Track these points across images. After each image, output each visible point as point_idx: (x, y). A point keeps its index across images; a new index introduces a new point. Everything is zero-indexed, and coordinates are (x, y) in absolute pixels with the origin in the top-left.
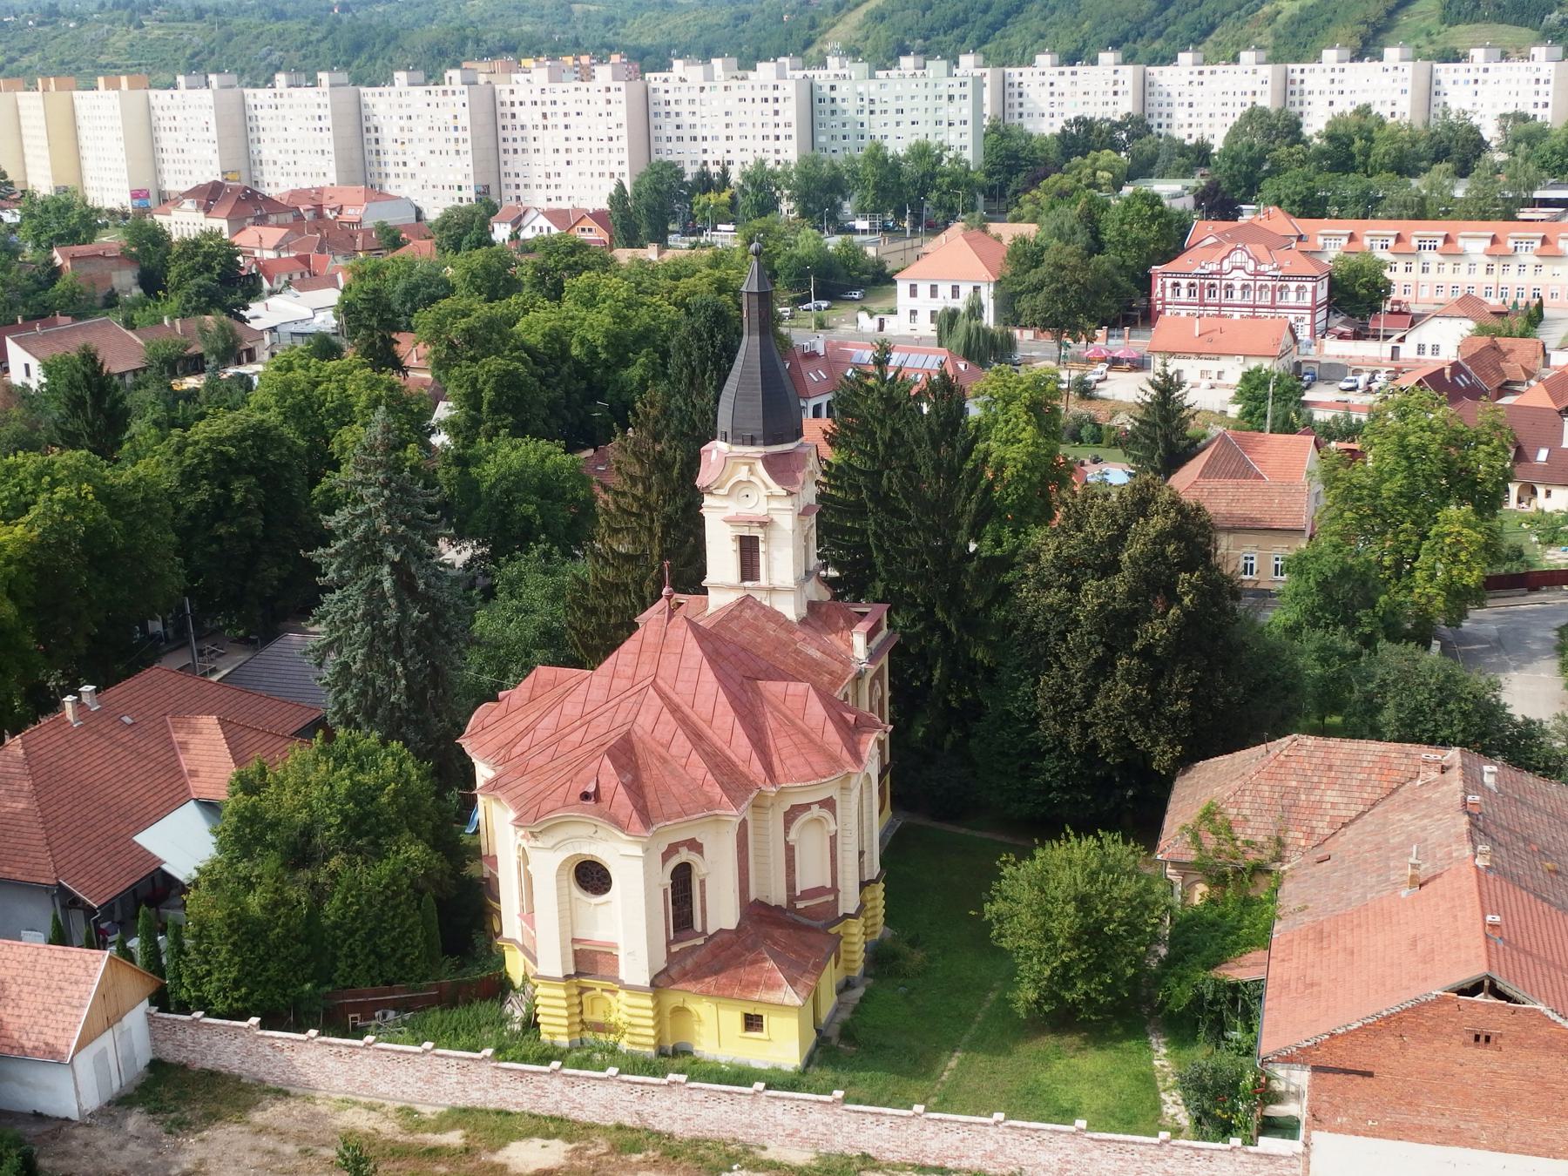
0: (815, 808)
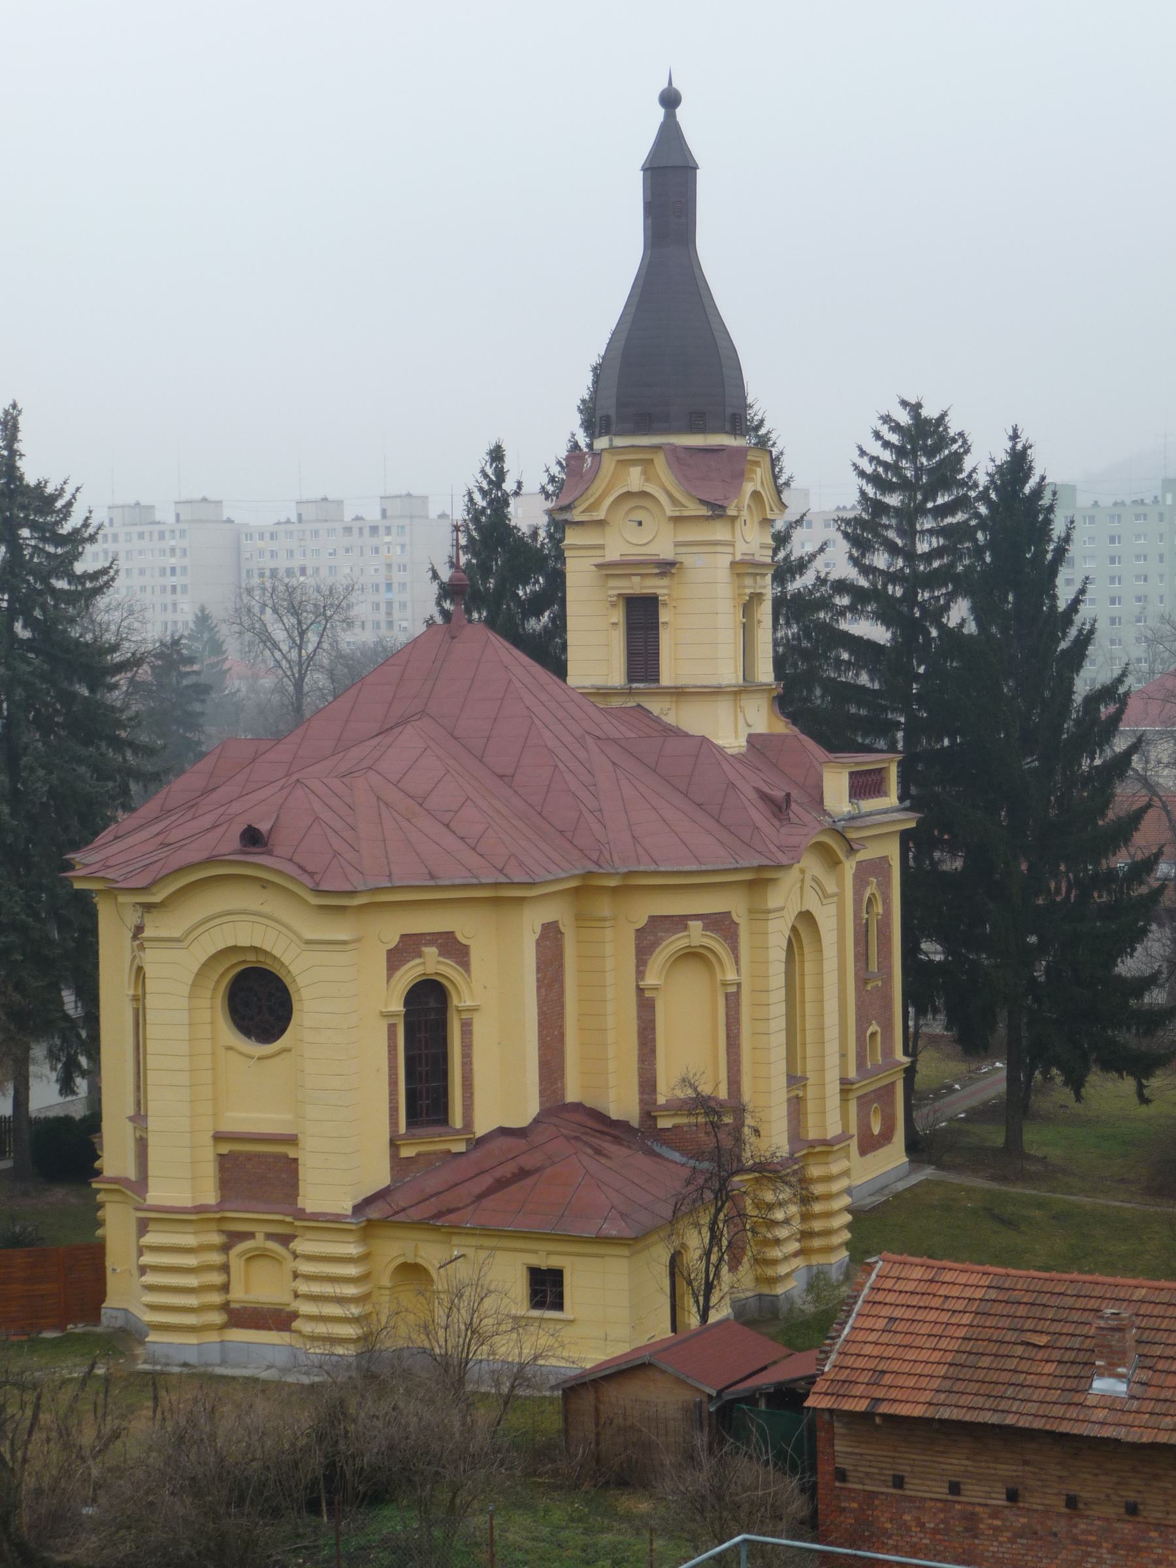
0: (696, 926)
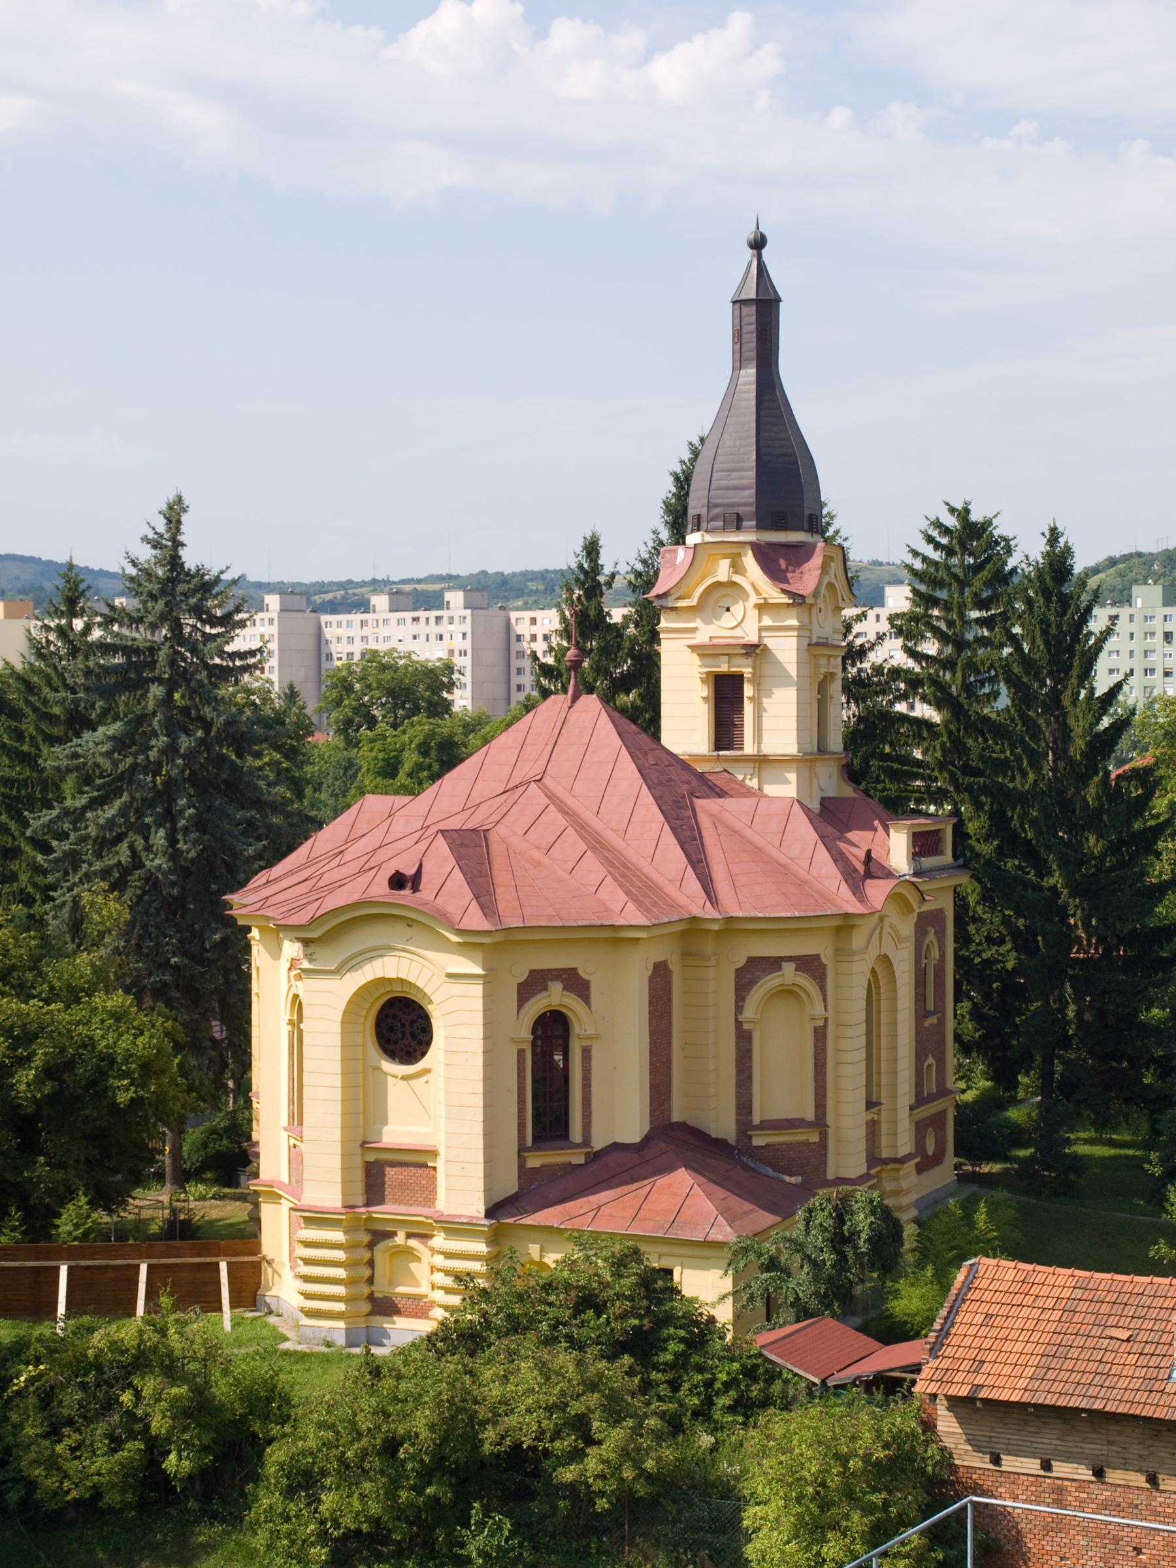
0: (789, 968)
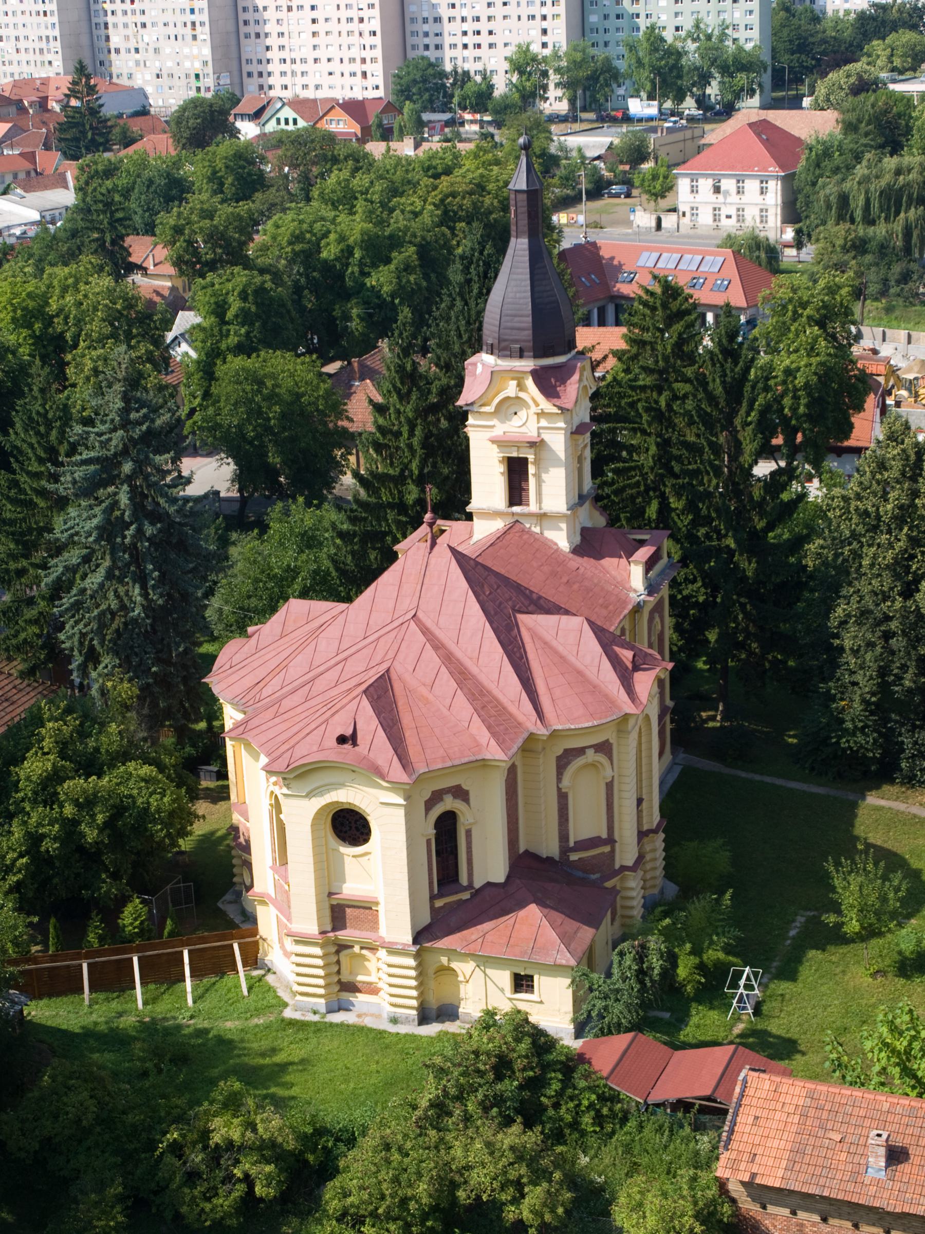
0: (590, 752)
